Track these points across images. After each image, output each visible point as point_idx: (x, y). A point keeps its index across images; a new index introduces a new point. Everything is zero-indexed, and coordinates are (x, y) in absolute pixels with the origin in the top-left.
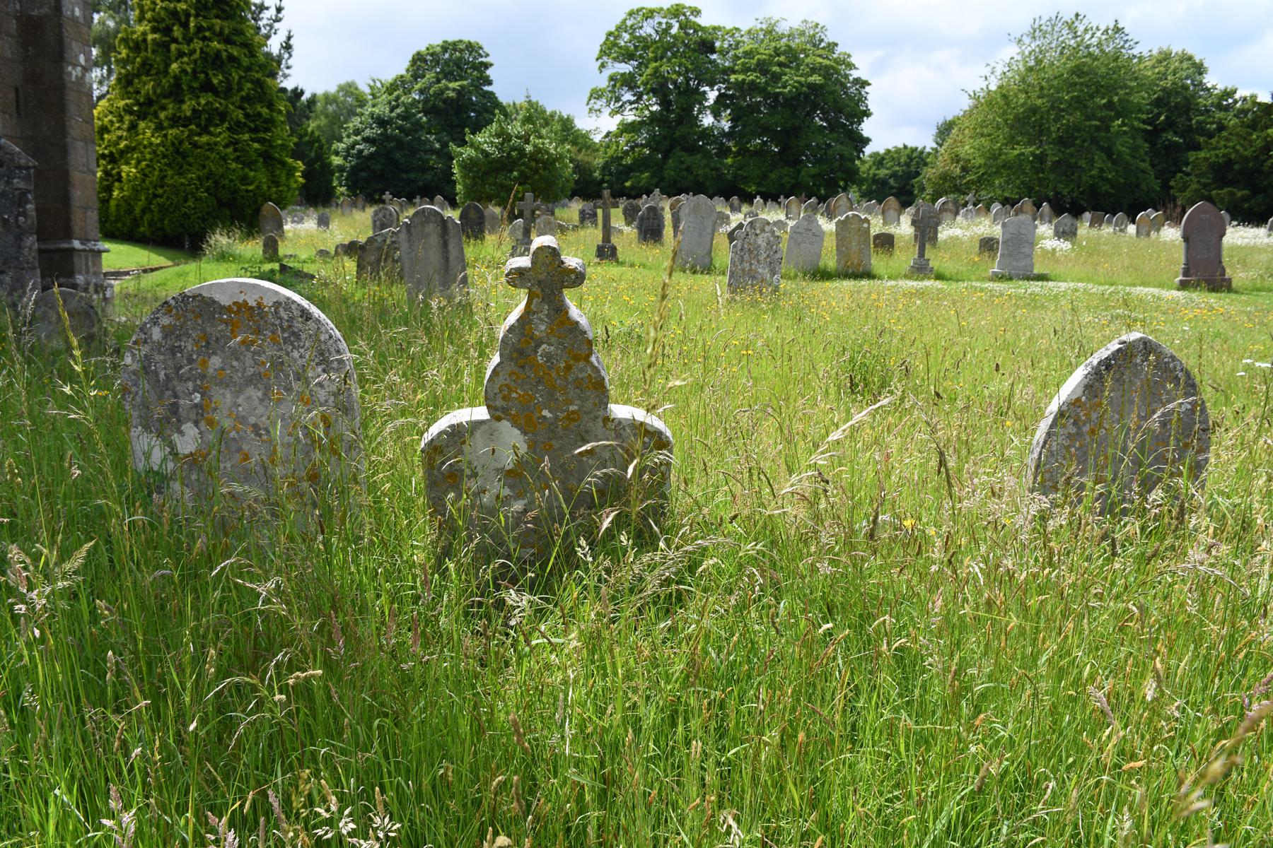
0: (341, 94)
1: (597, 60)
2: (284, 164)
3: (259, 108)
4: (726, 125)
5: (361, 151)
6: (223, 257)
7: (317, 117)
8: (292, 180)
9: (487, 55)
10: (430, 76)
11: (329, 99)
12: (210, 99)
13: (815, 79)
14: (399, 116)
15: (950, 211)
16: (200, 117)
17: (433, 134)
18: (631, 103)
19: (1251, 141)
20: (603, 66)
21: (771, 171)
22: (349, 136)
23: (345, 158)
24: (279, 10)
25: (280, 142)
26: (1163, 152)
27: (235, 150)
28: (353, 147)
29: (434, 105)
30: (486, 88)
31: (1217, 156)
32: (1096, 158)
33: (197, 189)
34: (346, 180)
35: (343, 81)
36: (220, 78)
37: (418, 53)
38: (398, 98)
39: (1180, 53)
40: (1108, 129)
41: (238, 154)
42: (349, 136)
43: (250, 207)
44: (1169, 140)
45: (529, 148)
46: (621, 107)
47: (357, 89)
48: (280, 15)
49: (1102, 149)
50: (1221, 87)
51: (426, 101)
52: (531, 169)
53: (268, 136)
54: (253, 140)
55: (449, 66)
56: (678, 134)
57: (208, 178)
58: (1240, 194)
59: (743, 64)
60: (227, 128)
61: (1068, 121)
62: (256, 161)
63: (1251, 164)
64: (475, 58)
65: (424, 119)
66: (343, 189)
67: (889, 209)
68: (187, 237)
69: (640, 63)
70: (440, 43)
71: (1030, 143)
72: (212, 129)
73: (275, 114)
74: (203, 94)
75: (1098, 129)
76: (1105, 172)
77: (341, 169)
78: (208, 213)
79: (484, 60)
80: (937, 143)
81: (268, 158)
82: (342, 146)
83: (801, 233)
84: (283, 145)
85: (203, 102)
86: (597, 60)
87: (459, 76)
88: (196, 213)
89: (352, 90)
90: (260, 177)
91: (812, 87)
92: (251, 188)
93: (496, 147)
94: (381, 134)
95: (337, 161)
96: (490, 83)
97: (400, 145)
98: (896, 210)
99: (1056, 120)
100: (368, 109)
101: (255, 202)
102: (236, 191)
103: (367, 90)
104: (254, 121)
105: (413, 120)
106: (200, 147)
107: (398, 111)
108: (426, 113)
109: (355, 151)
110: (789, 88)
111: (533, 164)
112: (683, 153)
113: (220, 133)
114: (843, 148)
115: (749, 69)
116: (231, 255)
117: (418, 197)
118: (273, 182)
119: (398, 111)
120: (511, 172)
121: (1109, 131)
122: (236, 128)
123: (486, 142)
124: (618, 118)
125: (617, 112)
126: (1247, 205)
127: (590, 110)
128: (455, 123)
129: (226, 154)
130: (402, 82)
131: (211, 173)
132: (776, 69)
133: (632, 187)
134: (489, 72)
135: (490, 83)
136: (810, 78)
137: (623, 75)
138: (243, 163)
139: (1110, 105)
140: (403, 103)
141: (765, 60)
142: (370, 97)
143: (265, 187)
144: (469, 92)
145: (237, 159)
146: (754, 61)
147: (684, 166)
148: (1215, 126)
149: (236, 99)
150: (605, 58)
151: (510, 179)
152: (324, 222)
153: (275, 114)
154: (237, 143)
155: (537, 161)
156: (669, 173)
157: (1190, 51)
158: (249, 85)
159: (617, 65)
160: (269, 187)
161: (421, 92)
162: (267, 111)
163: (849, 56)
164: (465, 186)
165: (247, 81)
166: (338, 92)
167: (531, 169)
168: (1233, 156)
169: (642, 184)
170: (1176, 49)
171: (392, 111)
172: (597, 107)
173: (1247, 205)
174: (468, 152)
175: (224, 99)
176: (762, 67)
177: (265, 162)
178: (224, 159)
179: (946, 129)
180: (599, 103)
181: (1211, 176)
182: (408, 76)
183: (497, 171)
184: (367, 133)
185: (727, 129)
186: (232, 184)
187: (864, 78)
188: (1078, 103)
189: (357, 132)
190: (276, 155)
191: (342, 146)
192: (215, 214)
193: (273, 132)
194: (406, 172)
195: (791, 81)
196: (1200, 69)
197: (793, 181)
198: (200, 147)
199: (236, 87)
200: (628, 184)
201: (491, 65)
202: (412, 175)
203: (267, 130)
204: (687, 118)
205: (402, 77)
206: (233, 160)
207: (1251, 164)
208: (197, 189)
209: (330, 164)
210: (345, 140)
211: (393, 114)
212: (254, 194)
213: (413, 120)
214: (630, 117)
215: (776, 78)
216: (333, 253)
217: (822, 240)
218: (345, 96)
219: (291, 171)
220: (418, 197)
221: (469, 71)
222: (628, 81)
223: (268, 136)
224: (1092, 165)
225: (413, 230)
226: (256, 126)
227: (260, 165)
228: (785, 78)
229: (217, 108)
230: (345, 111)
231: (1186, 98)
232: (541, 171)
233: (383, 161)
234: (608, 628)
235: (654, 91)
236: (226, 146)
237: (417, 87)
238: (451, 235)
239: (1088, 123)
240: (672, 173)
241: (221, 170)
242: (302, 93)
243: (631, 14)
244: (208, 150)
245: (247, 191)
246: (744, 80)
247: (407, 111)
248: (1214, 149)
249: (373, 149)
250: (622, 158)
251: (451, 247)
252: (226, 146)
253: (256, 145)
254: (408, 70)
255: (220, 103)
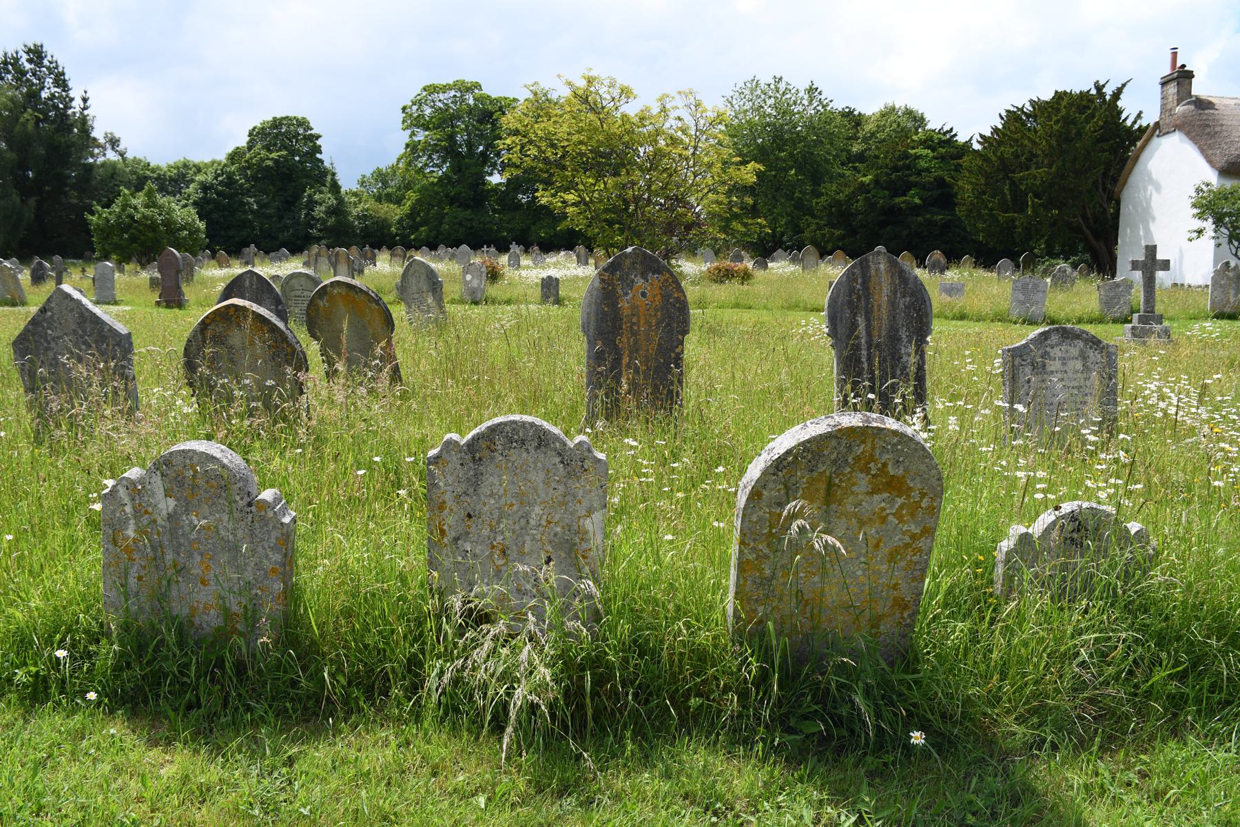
15: (400, 256)
21: (534, 224)
24: (85, 100)
39: (903, 108)
48: (88, 104)
70: (95, 125)
134: (318, 142)
170: (900, 104)
234: (1057, 691)
243: (425, 89)
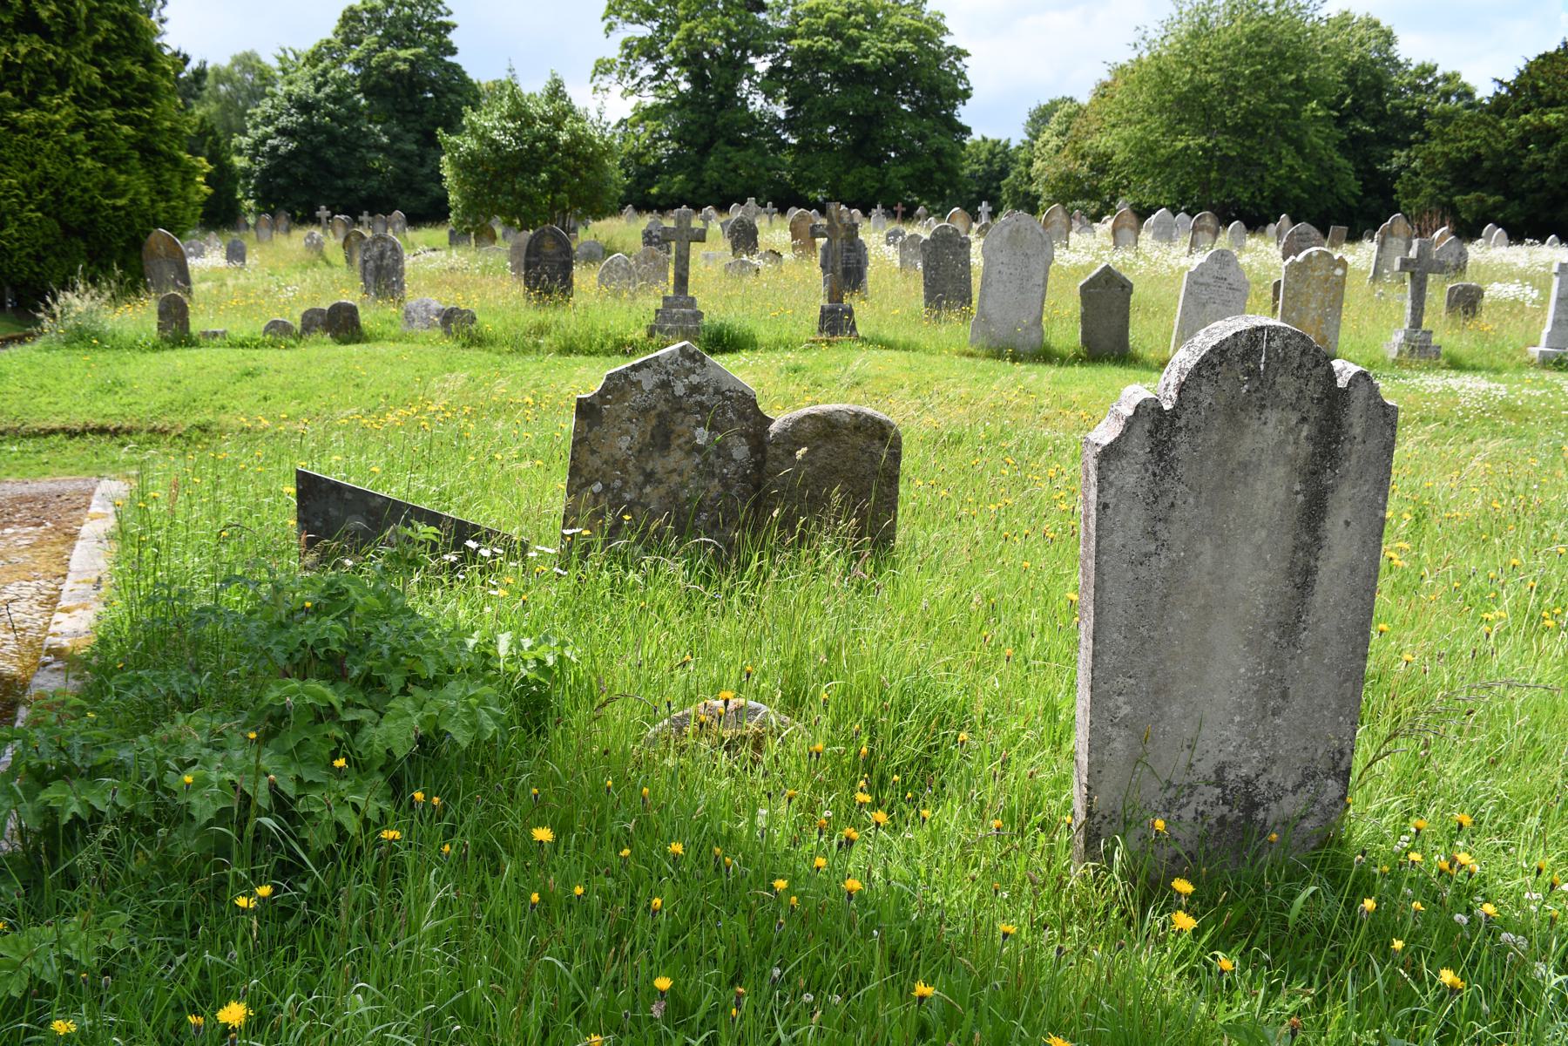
0: (237, 69)
1: (603, 19)
2: (176, 161)
3: (127, 64)
4: (781, 111)
5: (275, 148)
6: (83, 337)
7: (203, 102)
8: (192, 189)
9: (449, 13)
10: (370, 41)
11: (222, 77)
12: (37, 46)
13: (905, 45)
14: (328, 96)
15: (1208, 229)
16: (19, 78)
17: (377, 123)
18: (652, 79)
19: (1501, 130)
20: (610, 27)
21: (847, 172)
22: (256, 127)
23: (252, 159)
25: (167, 124)
26: (1350, 145)
27: (90, 137)
28: (263, 141)
29: (377, 83)
30: (448, 59)
31: (1459, 150)
32: (1284, 152)
33: (22, 205)
34: (255, 189)
35: (239, 51)
36: (53, 7)
37: (351, 9)
38: (325, 73)
39: (1364, 18)
40: (1296, 115)
41: (95, 143)
42: (256, 127)
43: (120, 235)
44: (1357, 130)
45: (563, 137)
46: (638, 85)
47: (259, 62)
49: (1291, 141)
50: (1416, 62)
51: (365, 77)
52: (565, 168)
53: (146, 113)
54: (120, 120)
55: (396, 27)
56: (720, 122)
57: (41, 187)
58: (1491, 200)
59: (809, 25)
60: (72, 98)
61: (1248, 102)
62: (127, 157)
63: (1505, 161)
64: (431, 17)
65: (363, 102)
66: (250, 203)
67: (1123, 227)
68: (8, 289)
69: (662, 25)
71: (1195, 135)
72: (43, 99)
73: (157, 76)
74: (21, 36)
75: (1284, 113)
76: (1296, 171)
77: (247, 174)
78: (46, 247)
79: (444, 19)
80: (1030, 135)
81: (148, 151)
82: (245, 141)
83: (1208, 285)
84: (172, 130)
85: (23, 50)
86: (603, 19)
87: (412, 41)
88: (22, 248)
89: (254, 62)
90: (137, 183)
91: (902, 57)
92: (121, 202)
93: (512, 135)
94: (304, 123)
95: (240, 162)
96: (453, 52)
97: (333, 140)
98: (1132, 228)
99: (1231, 103)
100: (281, 89)
101: (130, 227)
102: (93, 209)
103: (276, 64)
104: (120, 87)
105: (349, 103)
106: (24, 131)
107: (327, 90)
108: (368, 94)
109: (266, 149)
110: (872, 58)
111: (571, 161)
112: (729, 148)
113: (59, 106)
114: (942, 139)
115: (816, 33)
116: (95, 334)
117: (366, 213)
118: (159, 193)
119: (327, 90)
120: (537, 173)
121: (1298, 118)
122: (87, 98)
123: (494, 128)
124: (633, 100)
125: (632, 92)
126: (1501, 215)
127: (595, 88)
128: (408, 108)
129: (73, 144)
130: (329, 49)
131: (46, 179)
132: (853, 32)
133: (660, 196)
135: (453, 52)
136: (897, 45)
137: (641, 40)
138: (104, 159)
139: (1298, 83)
140: (333, 78)
141: (837, 19)
142: (281, 73)
143: (146, 200)
144: (428, 64)
145: (93, 153)
146: (824, 21)
147: (730, 166)
148: (1415, 112)
149: (86, 46)
150: (613, 17)
151: (536, 184)
152: (236, 254)
153: (157, 76)
154: (91, 125)
155: (576, 157)
156: (711, 175)
157: (1375, 16)
158: (107, 24)
159: (629, 26)
160: (153, 201)
161: (357, 63)
162: (142, 69)
163: (943, 17)
164: (464, 197)
165: (104, 17)
166: (233, 65)
167: (565, 168)
168: (1482, 151)
169: (673, 191)
171: (318, 90)
172: (603, 85)
173: (1501, 215)
174: (469, 143)
175: (64, 47)
176: (833, 30)
177: (143, 159)
178: (70, 151)
179: (1041, 117)
180: (607, 79)
181: (1448, 177)
182: (337, 42)
183: (515, 172)
184: (284, 121)
185: (782, 115)
186: (86, 197)
187: (961, 46)
188: (1257, 81)
189: (268, 120)
190: (163, 147)
191: (245, 141)
192: (58, 249)
193: (154, 107)
194: (342, 176)
195: (874, 49)
196: (1388, 38)
197: (877, 185)
198: (24, 131)
199: (83, 26)
200: (654, 191)
201: (455, 26)
202: (351, 182)
203: (144, 103)
204: (728, 98)
205: (329, 42)
206: (86, 155)
207: (1505, 161)
208: (22, 205)
209: (232, 165)
210: (250, 131)
211: (321, 95)
212: (128, 214)
213: (349, 103)
214: (649, 99)
215: (853, 44)
216: (298, 326)
217: (1246, 296)
218: (243, 71)
219: (188, 174)
220: (366, 213)
221: (423, 35)
222: (649, 50)
223: (146, 113)
224: (1280, 161)
225: (1182, 447)
226: (124, 96)
227: (135, 163)
228: (865, 44)
229: (50, 62)
230: (243, 94)
231: (1375, 76)
232: (583, 172)
233: (308, 162)
235: (683, 63)
236: (72, 130)
237: (352, 56)
238: (1351, 464)
239: (1273, 107)
240: (716, 175)
241: (65, 172)
242: (186, 60)
244: (39, 135)
245: (115, 208)
246: (810, 47)
247: (339, 91)
248: (1453, 141)
249: (293, 145)
250: (643, 155)
251: (1335, 526)
252: (72, 130)
253: (127, 129)
254: (336, 34)
255: (55, 54)
